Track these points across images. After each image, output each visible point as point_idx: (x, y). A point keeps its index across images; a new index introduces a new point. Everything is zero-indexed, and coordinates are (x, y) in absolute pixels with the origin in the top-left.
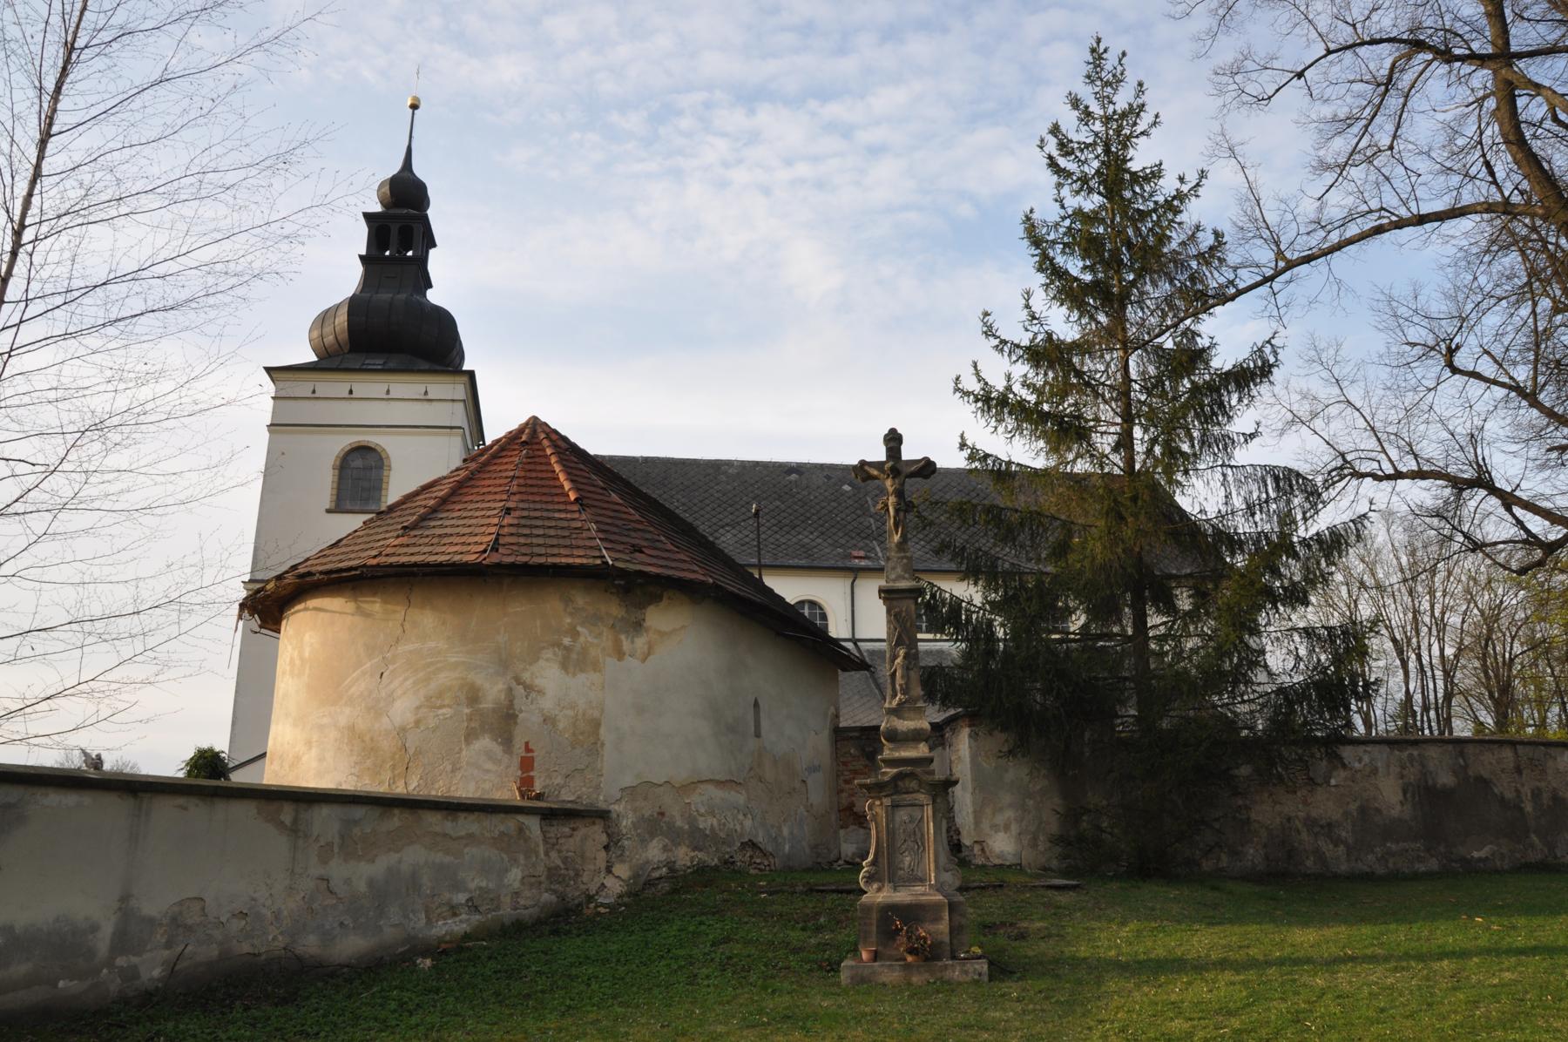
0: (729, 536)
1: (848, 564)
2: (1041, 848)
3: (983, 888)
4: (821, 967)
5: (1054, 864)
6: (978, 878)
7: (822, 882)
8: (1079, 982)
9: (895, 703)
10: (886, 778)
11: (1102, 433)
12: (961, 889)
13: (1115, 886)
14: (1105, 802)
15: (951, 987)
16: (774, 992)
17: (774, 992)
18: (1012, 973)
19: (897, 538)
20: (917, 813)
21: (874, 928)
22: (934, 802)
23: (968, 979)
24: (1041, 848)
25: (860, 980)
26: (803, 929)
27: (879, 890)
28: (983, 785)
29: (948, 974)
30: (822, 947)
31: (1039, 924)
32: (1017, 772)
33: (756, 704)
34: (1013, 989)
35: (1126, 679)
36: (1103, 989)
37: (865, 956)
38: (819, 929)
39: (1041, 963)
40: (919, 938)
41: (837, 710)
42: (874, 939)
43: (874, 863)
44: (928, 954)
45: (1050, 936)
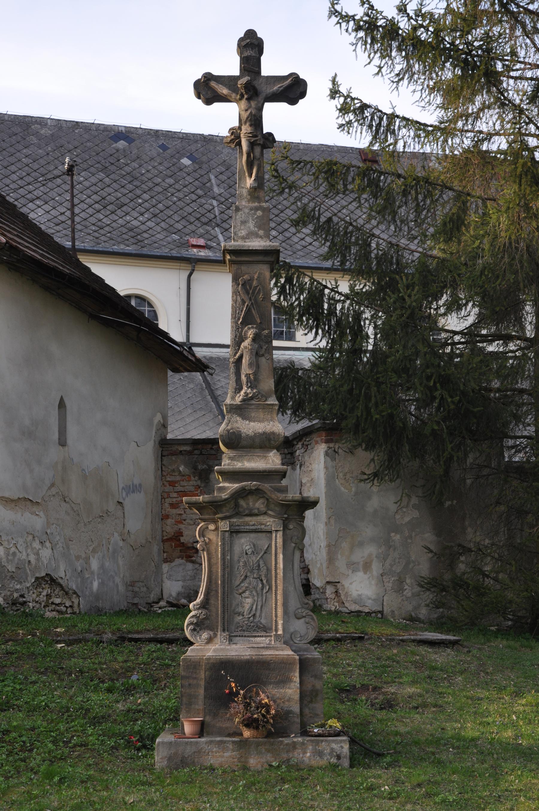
0: (40, 212)
1: (184, 253)
2: (408, 593)
3: (338, 640)
4: (129, 744)
5: (423, 613)
6: (333, 628)
7: (144, 627)
8: (470, 773)
9: (239, 399)
10: (224, 495)
11: (516, 78)
12: (317, 641)
13: (501, 643)
14: (487, 541)
15: (300, 774)
16: (61, 781)
17: (61, 781)
18: (380, 755)
19: (249, 182)
20: (262, 541)
21: (201, 691)
22: (285, 528)
23: (323, 762)
24: (408, 593)
25: (179, 762)
26: (109, 690)
27: (210, 640)
28: (342, 518)
29: (297, 756)
30: (133, 714)
31: (411, 690)
32: (382, 499)
33: (62, 405)
34: (380, 777)
35: (522, 391)
36: (504, 785)
37: (188, 728)
38: (130, 690)
39: (416, 743)
40: (260, 706)
41: (165, 417)
42: (200, 705)
43: (204, 605)
44: (272, 727)
45: (425, 705)
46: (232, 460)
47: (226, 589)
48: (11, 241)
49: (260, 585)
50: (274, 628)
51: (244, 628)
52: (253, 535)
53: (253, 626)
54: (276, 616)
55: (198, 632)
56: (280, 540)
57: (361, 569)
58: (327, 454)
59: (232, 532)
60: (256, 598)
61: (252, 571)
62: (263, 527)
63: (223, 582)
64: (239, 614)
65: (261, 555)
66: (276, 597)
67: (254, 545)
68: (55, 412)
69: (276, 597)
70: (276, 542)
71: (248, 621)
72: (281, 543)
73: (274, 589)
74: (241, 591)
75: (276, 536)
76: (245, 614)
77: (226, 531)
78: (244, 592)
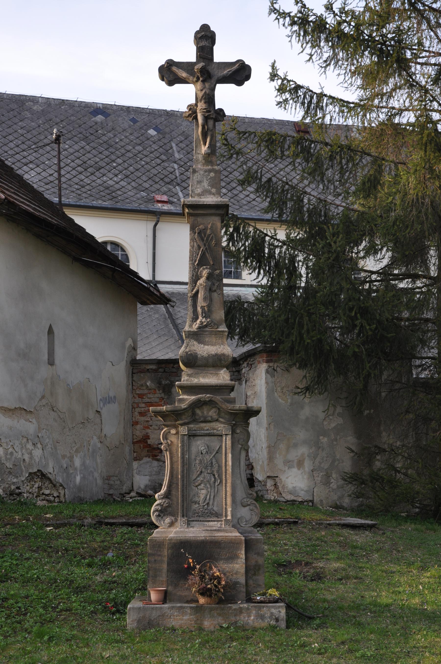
0: (33, 173)
1: (151, 207)
2: (334, 485)
3: (277, 524)
4: (105, 609)
5: (346, 502)
6: (273, 514)
7: (118, 513)
8: (384, 633)
9: (195, 326)
10: (184, 406)
12: (259, 525)
13: (410, 527)
14: (398, 443)
15: (245, 634)
16: (50, 639)
17: (50, 639)
18: (311, 618)
19: (204, 149)
20: (214, 443)
21: (165, 566)
22: (233, 432)
23: (264, 624)
24: (334, 485)
25: (147, 624)
26: (90, 565)
27: (172, 524)
28: (280, 424)
29: (243, 619)
30: (109, 585)
31: (336, 565)
32: (313, 408)
33: (51, 331)
34: (311, 636)
35: (427, 320)
36: (412, 643)
37: (154, 596)
38: (106, 565)
39: (341, 608)
40: (213, 578)
41: (135, 342)
42: (164, 577)
43: (167, 496)
44: (222, 595)
45: (348, 577)
46: (190, 377)
47: (185, 482)
48: (9, 198)
49: (213, 479)
50: (224, 514)
51: (199, 515)
52: (207, 438)
53: (207, 513)
54: (226, 505)
55: (162, 518)
56: (229, 442)
57: (296, 466)
58: (267, 372)
59: (189, 436)
60: (209, 490)
61: (206, 468)
62: (215, 431)
63: (183, 476)
64: (196, 503)
65: (213, 454)
66: (226, 489)
67: (208, 447)
68: (45, 338)
69: (226, 489)
70: (226, 443)
71: (203, 508)
72: (230, 445)
73: (224, 482)
74: (197, 484)
75: (226, 439)
76: (200, 502)
77: (185, 435)
78: (199, 485)
